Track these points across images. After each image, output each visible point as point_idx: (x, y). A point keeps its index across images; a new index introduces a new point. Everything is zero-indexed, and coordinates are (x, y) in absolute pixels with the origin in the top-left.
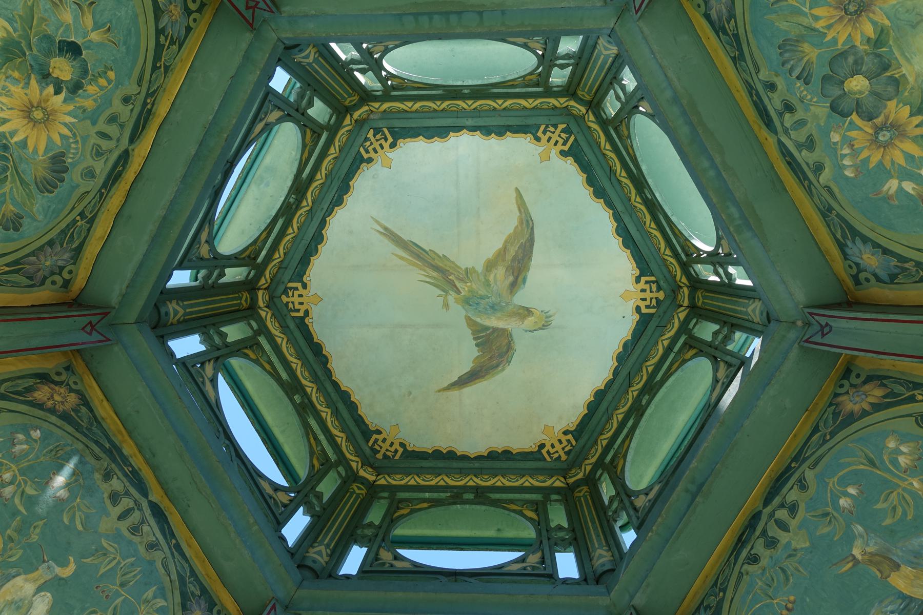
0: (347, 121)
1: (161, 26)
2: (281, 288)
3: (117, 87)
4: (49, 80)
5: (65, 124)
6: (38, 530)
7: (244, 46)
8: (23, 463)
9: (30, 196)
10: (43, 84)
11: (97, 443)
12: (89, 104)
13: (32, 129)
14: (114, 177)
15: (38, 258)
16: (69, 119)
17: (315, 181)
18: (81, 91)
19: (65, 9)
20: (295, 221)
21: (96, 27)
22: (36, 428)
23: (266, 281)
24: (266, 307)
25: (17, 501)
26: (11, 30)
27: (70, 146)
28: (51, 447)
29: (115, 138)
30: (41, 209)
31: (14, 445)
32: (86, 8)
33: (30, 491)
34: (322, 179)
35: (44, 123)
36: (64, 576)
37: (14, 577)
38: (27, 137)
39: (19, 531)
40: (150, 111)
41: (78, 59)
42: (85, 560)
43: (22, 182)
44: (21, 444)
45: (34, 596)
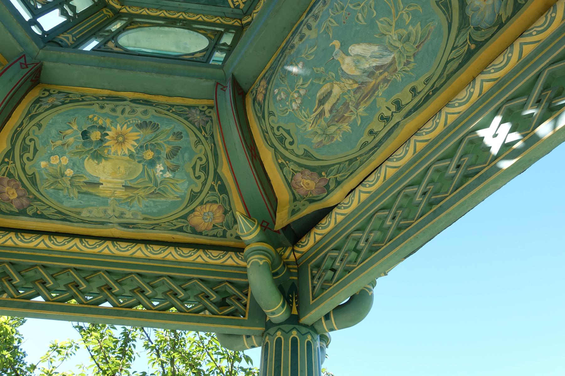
0: (124, 11)
1: (61, 104)
2: (236, 11)
3: (97, 113)
4: (103, 139)
5: (122, 128)
6: (318, 69)
7: (52, 64)
8: (289, 91)
9: (162, 132)
10: (106, 141)
11: (279, 61)
12: (108, 121)
13: (129, 139)
14: (147, 103)
15: (196, 122)
16: (119, 127)
17: (166, 16)
18: (103, 126)
19: (68, 142)
20: (194, 19)
21: (70, 128)
22: (274, 92)
23: (236, 22)
24: (251, 16)
25: (306, 86)
26: (87, 158)
27: (132, 123)
28: (281, 82)
29: (124, 107)
30: (168, 127)
31: (282, 99)
32: (64, 134)
33: (301, 82)
34: (163, 12)
35: (124, 136)
36: (340, 44)
37: (343, 70)
38: (133, 140)
39: (320, 79)
40: (107, 97)
41: (88, 130)
42: (331, 37)
43: (156, 137)
44: (281, 96)
45: (351, 56)
